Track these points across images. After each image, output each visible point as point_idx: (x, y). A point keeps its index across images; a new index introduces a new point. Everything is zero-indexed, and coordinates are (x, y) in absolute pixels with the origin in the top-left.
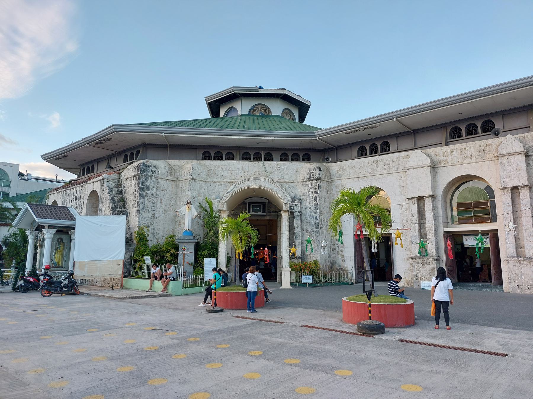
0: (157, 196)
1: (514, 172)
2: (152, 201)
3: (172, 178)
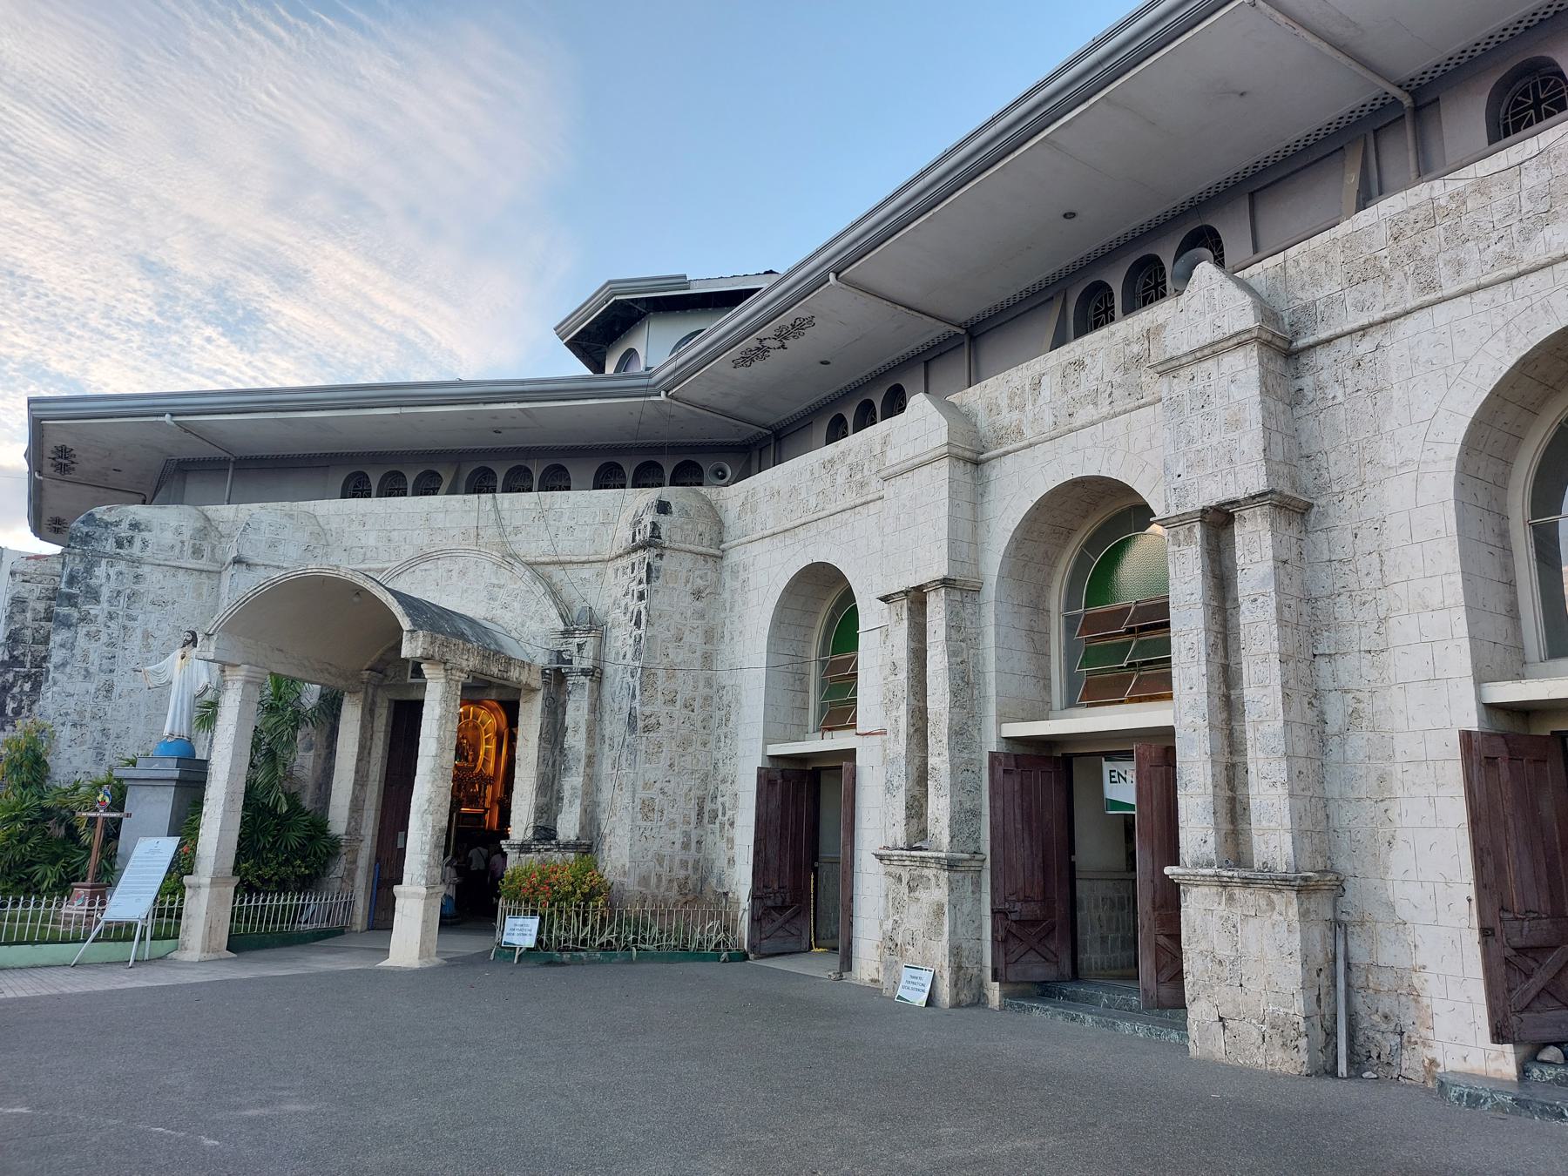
0: (129, 624)
1: (1214, 440)
2: (104, 638)
3: (202, 564)
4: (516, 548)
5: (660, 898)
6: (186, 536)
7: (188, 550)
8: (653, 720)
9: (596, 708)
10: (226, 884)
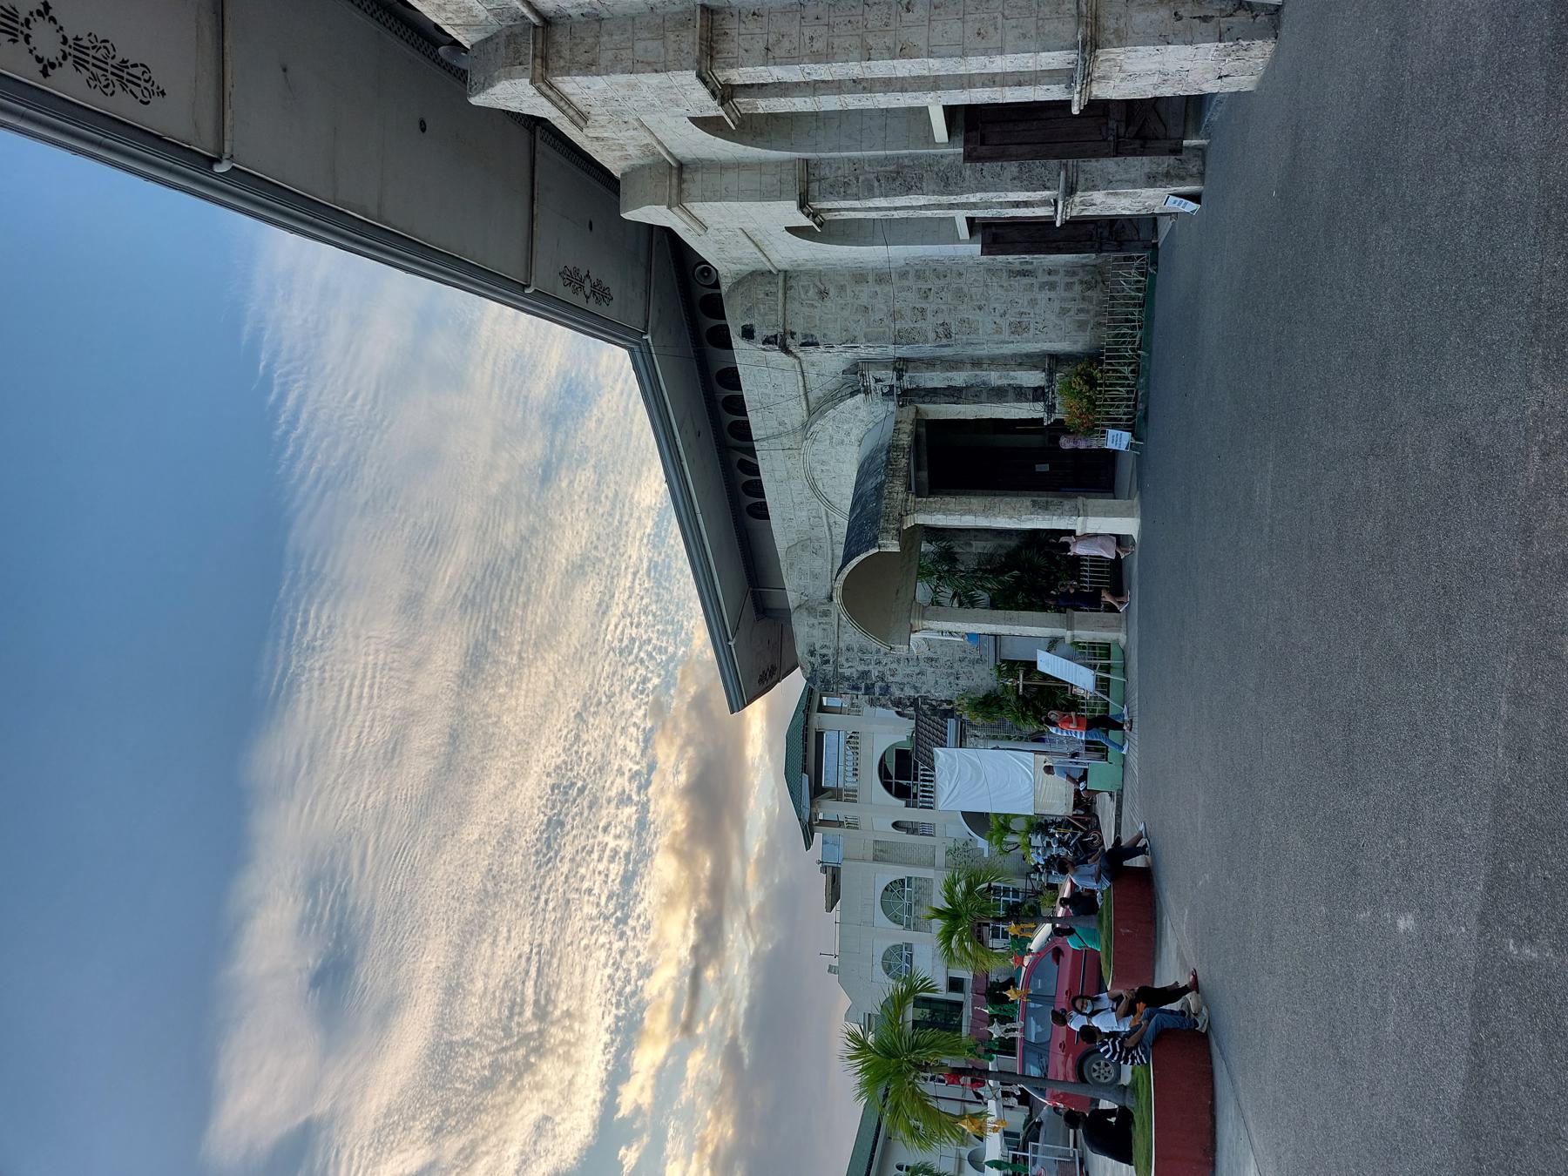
2: (894, 666)
4: (797, 424)
5: (1098, 309)
6: (812, 621)
7: (824, 620)
8: (940, 330)
9: (931, 363)
10: (1072, 617)
